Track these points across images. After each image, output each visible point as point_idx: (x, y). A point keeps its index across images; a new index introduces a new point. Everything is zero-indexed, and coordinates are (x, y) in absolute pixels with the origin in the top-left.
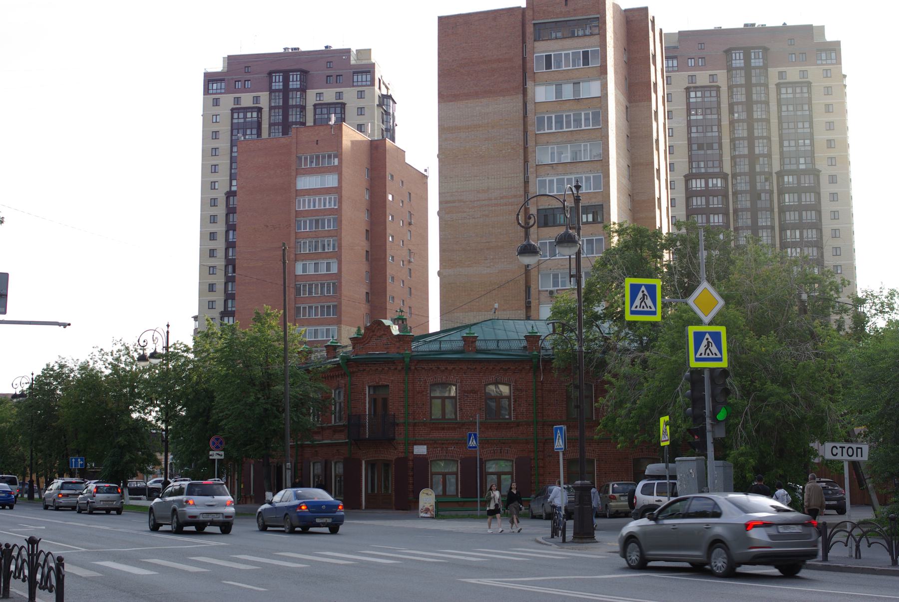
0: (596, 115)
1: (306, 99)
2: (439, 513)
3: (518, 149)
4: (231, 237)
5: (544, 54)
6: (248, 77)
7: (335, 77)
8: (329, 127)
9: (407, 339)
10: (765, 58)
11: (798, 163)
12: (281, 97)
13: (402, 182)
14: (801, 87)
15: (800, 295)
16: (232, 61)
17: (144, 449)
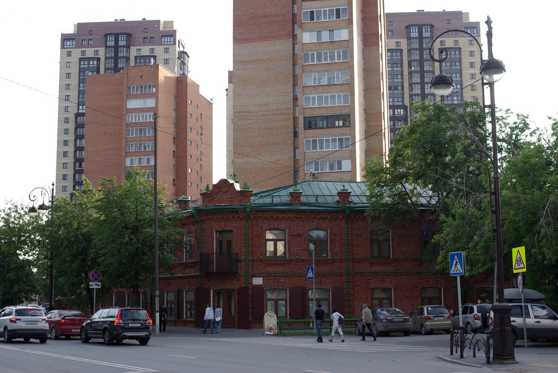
0: (345, 52)
1: (129, 53)
2: (282, 331)
3: (289, 76)
4: (78, 143)
5: (309, 10)
6: (91, 37)
7: (149, 38)
8: (150, 67)
9: (247, 194)
10: (432, 32)
11: (453, 100)
12: (113, 51)
13: (197, 106)
14: (455, 51)
15: (44, 279)
16: (80, 26)
17: (29, 282)
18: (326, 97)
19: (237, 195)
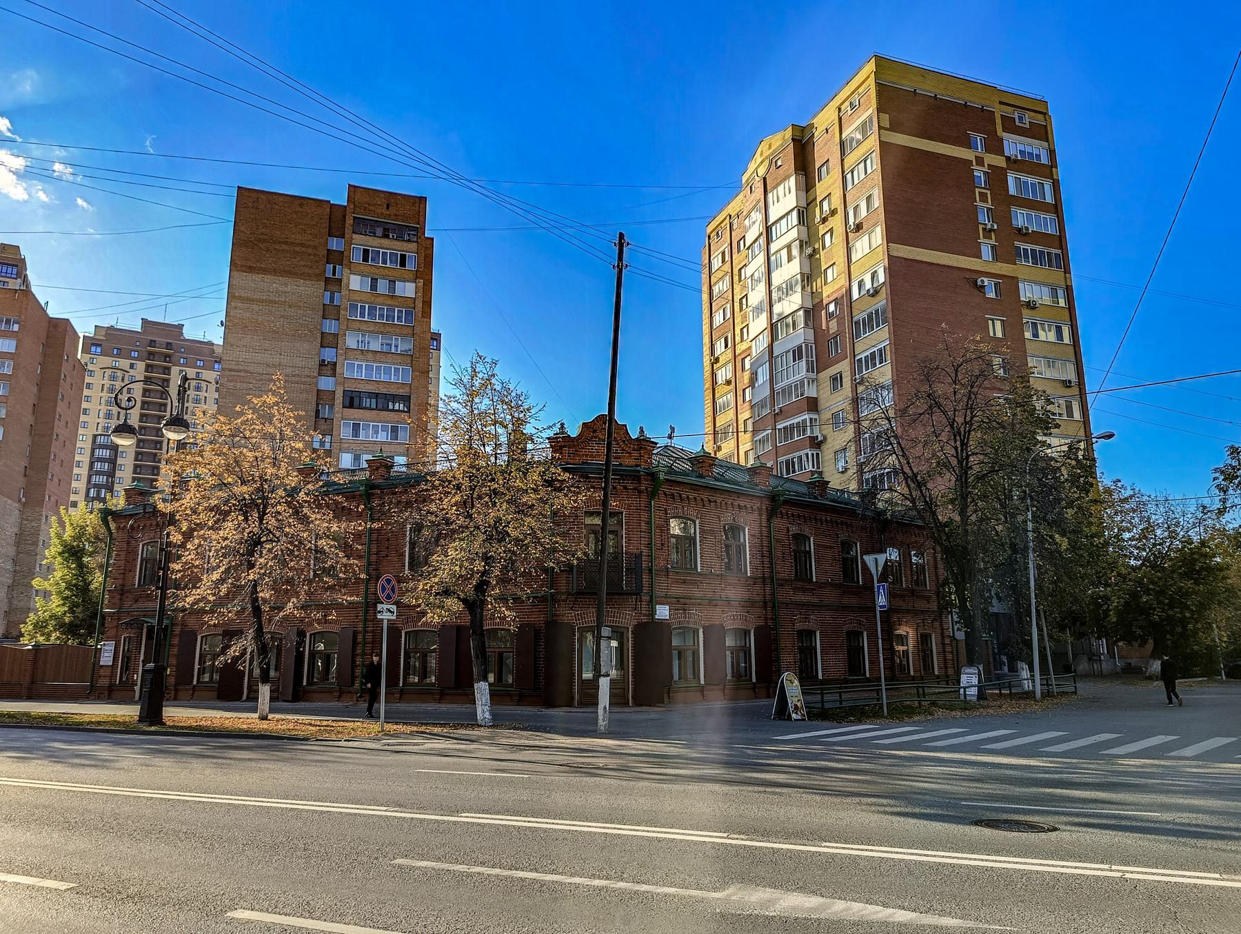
19: (630, 447)
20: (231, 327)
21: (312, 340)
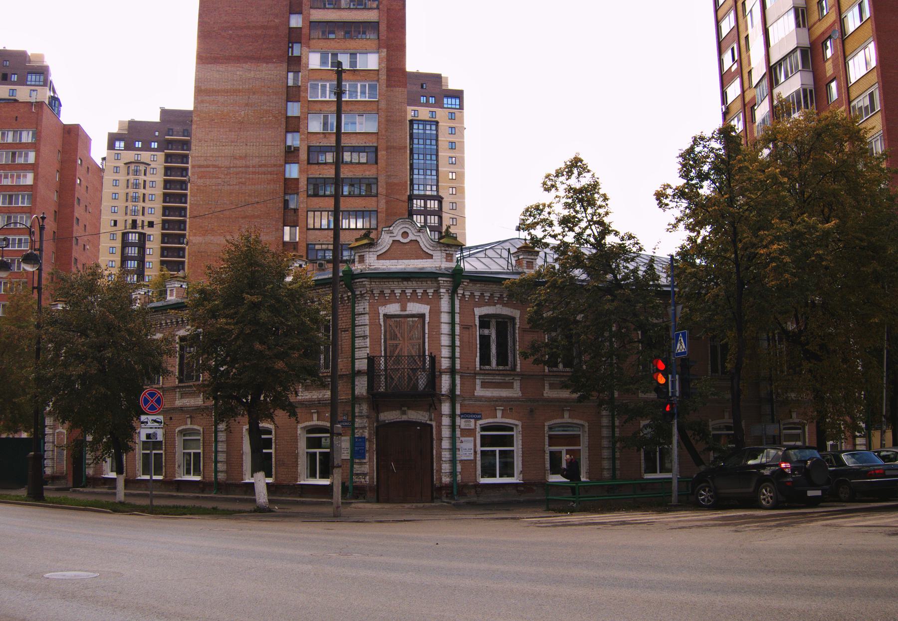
18: (20, 240)
20: (198, 122)
21: (277, 126)
